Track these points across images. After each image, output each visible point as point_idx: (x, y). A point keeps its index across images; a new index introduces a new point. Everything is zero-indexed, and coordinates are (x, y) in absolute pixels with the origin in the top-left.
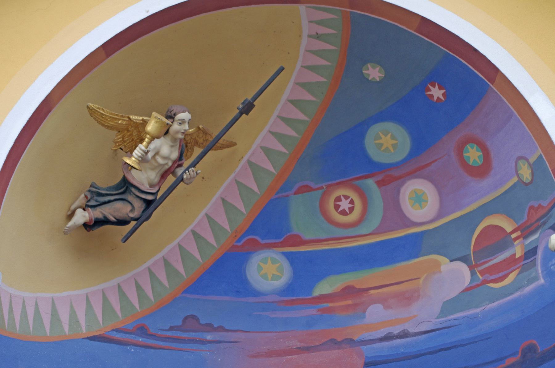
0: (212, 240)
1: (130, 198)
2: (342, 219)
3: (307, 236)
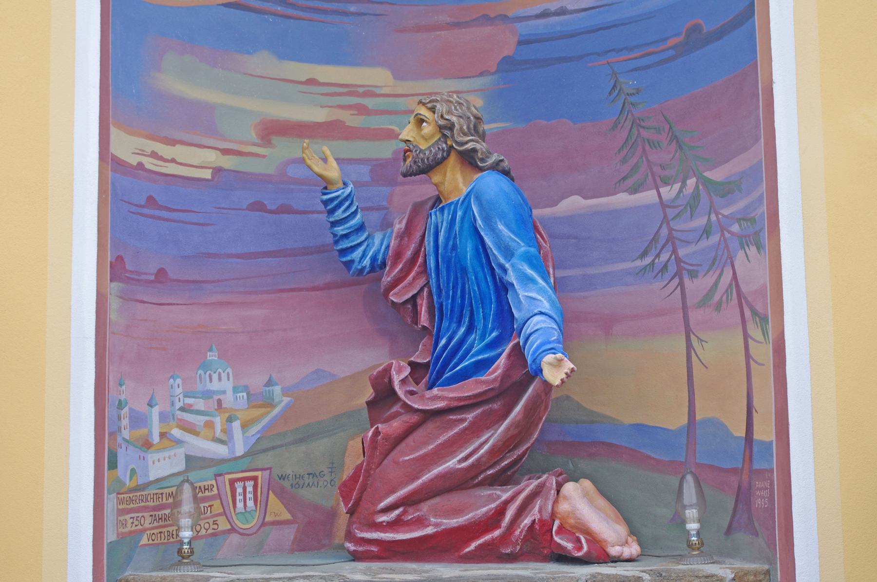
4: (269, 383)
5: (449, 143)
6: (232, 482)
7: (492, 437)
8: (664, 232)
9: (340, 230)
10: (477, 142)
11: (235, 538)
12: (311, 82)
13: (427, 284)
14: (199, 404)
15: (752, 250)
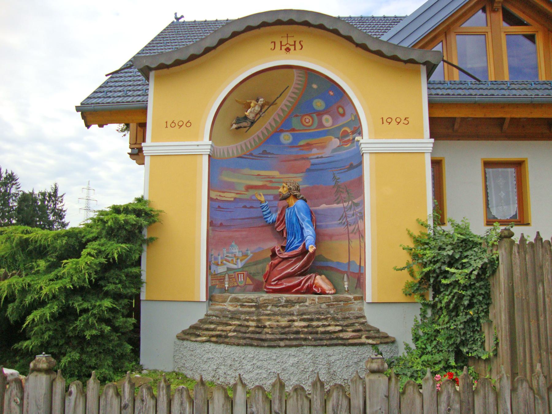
0: (271, 130)
2: (307, 124)
3: (297, 129)
4: (247, 250)
7: (299, 264)
9: (265, 213)
11: (238, 288)
12: (259, 175)
14: (230, 255)
15: (361, 220)
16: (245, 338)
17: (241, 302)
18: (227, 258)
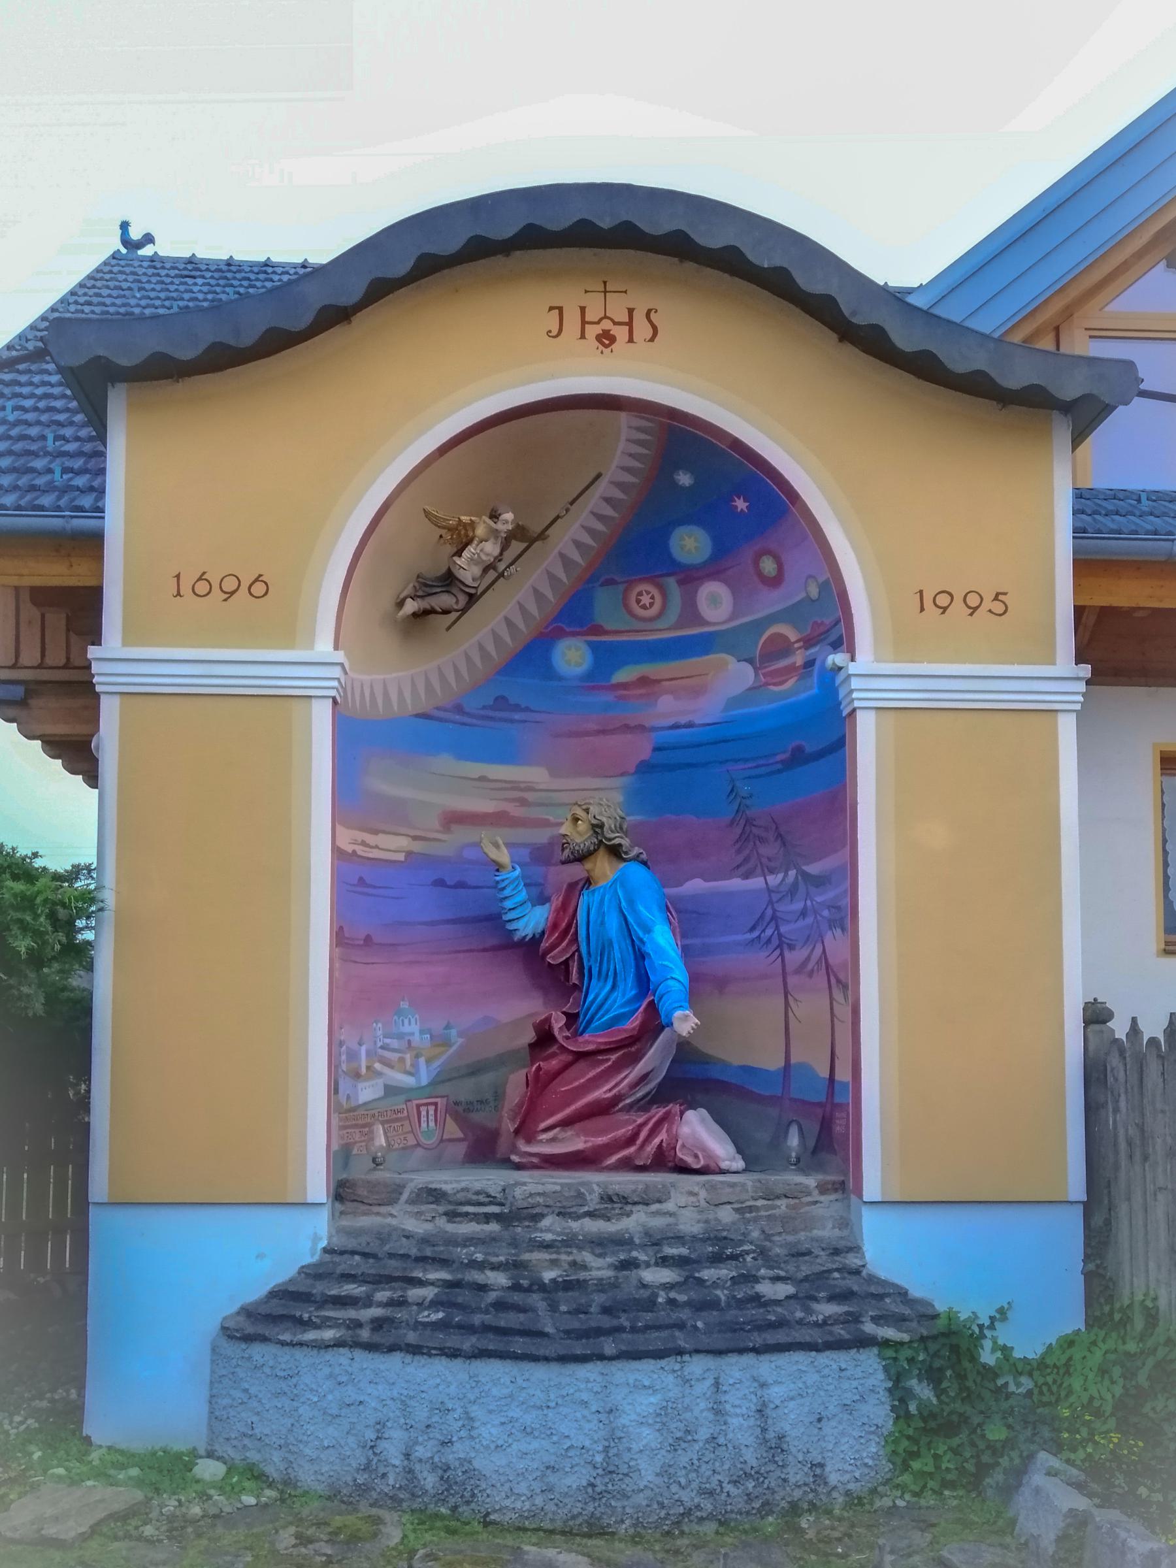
1: (454, 591)
3: (608, 627)
5: (600, 838)
6: (418, 1106)
8: (769, 912)
10: (622, 838)
11: (420, 1152)
12: (482, 779)
13: (578, 950)
14: (394, 1043)
15: (838, 932)
16: (469, 1329)
17: (450, 1202)
18: (387, 1054)
